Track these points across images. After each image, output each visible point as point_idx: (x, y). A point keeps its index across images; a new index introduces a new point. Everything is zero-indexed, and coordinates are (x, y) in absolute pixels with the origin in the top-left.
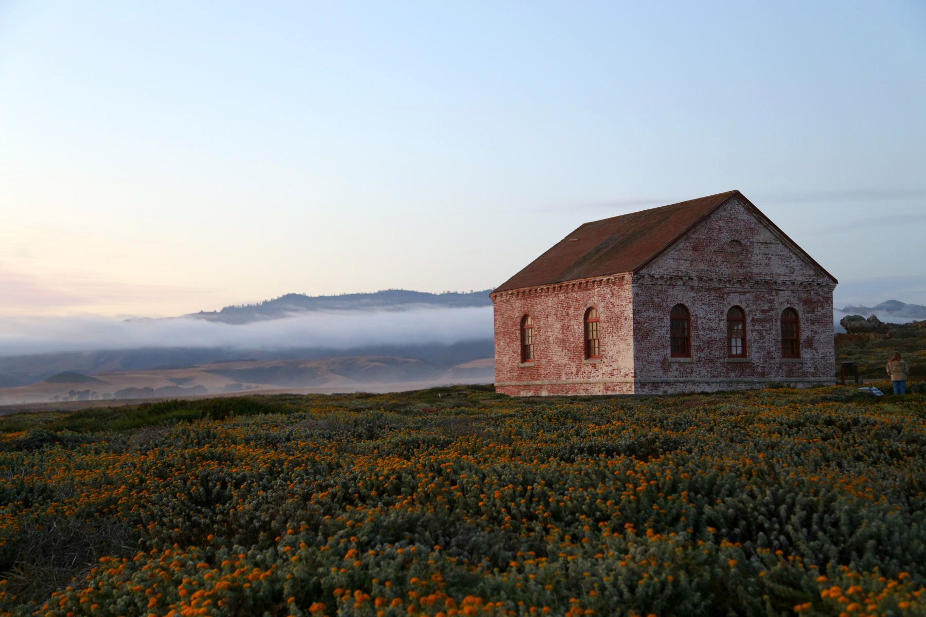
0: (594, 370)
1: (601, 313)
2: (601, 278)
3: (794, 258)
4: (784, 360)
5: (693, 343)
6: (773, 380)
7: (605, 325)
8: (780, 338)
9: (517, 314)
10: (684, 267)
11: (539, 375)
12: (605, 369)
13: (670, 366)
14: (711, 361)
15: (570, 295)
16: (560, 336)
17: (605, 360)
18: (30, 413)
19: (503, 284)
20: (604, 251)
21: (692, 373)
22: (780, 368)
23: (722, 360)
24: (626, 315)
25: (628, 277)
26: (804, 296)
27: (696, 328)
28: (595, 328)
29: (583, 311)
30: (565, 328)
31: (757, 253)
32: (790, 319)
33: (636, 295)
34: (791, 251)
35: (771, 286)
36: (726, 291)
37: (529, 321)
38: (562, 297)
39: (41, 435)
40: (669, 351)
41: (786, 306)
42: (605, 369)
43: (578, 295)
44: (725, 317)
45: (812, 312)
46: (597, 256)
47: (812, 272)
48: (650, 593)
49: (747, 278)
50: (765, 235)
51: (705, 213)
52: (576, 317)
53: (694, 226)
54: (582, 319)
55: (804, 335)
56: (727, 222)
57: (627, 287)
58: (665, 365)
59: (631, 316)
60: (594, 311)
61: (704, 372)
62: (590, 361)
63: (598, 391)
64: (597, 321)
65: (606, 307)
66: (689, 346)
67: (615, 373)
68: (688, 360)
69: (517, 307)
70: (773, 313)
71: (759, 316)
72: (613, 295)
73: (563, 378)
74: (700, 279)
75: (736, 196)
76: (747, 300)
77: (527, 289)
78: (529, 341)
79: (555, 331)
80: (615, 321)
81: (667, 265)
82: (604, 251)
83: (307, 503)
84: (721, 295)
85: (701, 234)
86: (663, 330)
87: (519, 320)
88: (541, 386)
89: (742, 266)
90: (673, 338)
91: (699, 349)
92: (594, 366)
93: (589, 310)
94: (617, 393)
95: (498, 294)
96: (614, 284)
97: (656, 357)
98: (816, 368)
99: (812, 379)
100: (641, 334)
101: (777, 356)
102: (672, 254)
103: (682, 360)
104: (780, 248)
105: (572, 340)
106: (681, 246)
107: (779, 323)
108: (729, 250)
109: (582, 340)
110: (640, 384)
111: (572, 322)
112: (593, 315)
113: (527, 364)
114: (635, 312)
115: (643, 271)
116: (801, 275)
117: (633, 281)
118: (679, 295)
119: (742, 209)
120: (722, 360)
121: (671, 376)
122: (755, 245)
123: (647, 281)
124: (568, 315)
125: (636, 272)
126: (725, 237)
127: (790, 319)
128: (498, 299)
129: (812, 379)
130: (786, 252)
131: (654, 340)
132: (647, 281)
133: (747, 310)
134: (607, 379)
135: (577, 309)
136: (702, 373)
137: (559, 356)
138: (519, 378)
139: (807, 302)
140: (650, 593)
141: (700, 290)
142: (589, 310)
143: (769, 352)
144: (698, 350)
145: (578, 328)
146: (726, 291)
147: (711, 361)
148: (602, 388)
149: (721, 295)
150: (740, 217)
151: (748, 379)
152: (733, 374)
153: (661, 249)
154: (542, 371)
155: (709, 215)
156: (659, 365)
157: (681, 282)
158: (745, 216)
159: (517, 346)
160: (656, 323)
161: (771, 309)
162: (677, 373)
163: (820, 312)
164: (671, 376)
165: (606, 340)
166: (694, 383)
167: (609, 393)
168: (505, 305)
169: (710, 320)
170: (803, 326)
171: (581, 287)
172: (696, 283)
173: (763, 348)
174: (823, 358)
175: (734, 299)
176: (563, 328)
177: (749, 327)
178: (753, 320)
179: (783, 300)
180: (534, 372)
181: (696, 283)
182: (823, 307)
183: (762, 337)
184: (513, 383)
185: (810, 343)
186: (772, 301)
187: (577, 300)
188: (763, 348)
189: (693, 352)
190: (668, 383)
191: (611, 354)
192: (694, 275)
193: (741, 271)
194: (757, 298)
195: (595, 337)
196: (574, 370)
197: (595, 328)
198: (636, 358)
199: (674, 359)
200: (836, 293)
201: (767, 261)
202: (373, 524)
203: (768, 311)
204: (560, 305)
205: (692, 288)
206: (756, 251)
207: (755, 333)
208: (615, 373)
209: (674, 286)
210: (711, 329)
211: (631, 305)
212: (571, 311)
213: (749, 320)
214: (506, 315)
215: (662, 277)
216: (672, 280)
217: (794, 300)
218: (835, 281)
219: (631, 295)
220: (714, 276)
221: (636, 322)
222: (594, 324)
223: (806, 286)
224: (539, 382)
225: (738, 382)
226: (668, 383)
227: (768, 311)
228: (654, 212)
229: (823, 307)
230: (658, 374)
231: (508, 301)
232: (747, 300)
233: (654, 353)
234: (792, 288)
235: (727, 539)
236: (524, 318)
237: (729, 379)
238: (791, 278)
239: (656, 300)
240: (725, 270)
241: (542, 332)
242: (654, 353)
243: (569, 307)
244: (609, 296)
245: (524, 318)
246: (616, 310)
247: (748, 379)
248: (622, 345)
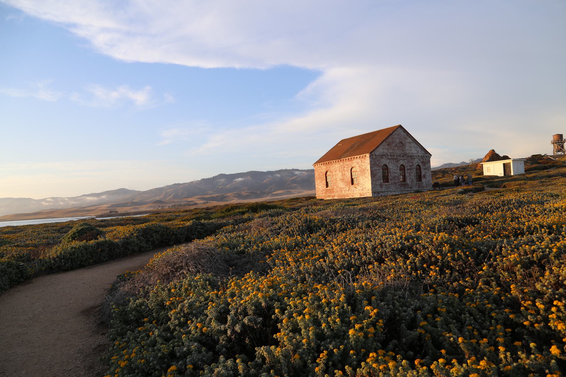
0: (355, 189)
1: (357, 169)
2: (357, 156)
3: (419, 148)
4: (417, 182)
5: (389, 178)
6: (414, 189)
7: (359, 173)
8: (416, 175)
9: (324, 171)
10: (386, 151)
11: (334, 192)
12: (360, 188)
13: (383, 186)
14: (395, 184)
15: (344, 163)
16: (341, 178)
17: (359, 185)
18: (159, 213)
19: (254, 171)
20: (354, 148)
21: (389, 188)
22: (416, 185)
23: (399, 183)
24: (367, 169)
25: (368, 155)
26: (422, 160)
27: (390, 172)
28: (355, 174)
31: (408, 145)
32: (419, 168)
33: (371, 162)
34: (417, 145)
35: (412, 157)
36: (399, 159)
37: (328, 173)
38: (341, 164)
39: (196, 223)
40: (382, 181)
41: (417, 164)
42: (360, 188)
43: (348, 163)
44: (399, 168)
45: (425, 166)
46: (352, 149)
47: (424, 152)
49: (405, 155)
50: (409, 140)
51: (391, 133)
52: (347, 171)
53: (388, 137)
54: (350, 171)
55: (423, 174)
56: (398, 136)
57: (367, 159)
58: (381, 186)
59: (370, 169)
60: (354, 168)
61: (393, 188)
62: (353, 186)
63: (357, 196)
65: (360, 167)
66: (388, 179)
67: (364, 189)
68: (388, 184)
70: (413, 166)
71: (409, 168)
72: (362, 162)
73: (343, 192)
74: (391, 156)
76: (405, 162)
77: (327, 162)
79: (339, 175)
81: (380, 151)
82: (354, 148)
84: (397, 160)
85: (390, 140)
86: (380, 174)
87: (325, 173)
88: (334, 196)
89: (403, 151)
90: (383, 176)
91: (392, 180)
92: (355, 187)
94: (365, 196)
95: (316, 164)
96: (362, 158)
97: (378, 183)
98: (426, 185)
99: (426, 188)
100: (373, 175)
101: (415, 181)
102: (381, 147)
103: (386, 184)
104: (414, 144)
105: (346, 179)
106: (384, 144)
107: (415, 170)
108: (399, 145)
109: (350, 178)
110: (373, 193)
111: (346, 173)
113: (328, 188)
114: (371, 168)
115: (372, 153)
116: (421, 153)
117: (370, 156)
118: (385, 161)
119: (402, 131)
120: (399, 183)
121: (384, 189)
122: (407, 143)
123: (374, 156)
124: (344, 170)
126: (398, 141)
127: (419, 168)
128: (316, 166)
129: (426, 188)
130: (416, 146)
131: (377, 177)
132: (374, 156)
133: (405, 166)
134: (360, 191)
135: (347, 168)
136: (393, 188)
137: (341, 185)
138: (326, 193)
139: (423, 162)
141: (390, 159)
143: (413, 180)
144: (391, 180)
146: (399, 159)
147: (395, 184)
148: (359, 195)
149: (397, 160)
150: (402, 134)
151: (406, 189)
152: (402, 188)
153: (378, 145)
154: (335, 190)
155: (392, 133)
156: (379, 186)
157: (384, 157)
160: (377, 171)
161: (413, 165)
162: (385, 188)
163: (427, 165)
164: (384, 189)
165: (360, 178)
166: (390, 191)
167: (362, 196)
168: (319, 168)
169: (394, 169)
170: (422, 171)
172: (389, 157)
173: (411, 178)
174: (428, 181)
175: (401, 162)
176: (342, 175)
177: (406, 171)
178: (407, 169)
179: (416, 162)
180: (332, 191)
181: (389, 157)
182: (427, 164)
183: (410, 175)
184: (324, 195)
185: (424, 176)
186: (412, 163)
187: (347, 165)
188: (411, 178)
189: (390, 181)
190: (382, 192)
191: (362, 183)
192: (389, 154)
193: (403, 152)
194: (408, 162)
195: (355, 177)
196: (347, 189)
197: (355, 174)
198: (372, 184)
199: (384, 184)
200: (432, 159)
201: (410, 149)
203: (411, 166)
204: (341, 167)
205: (388, 158)
206: (407, 145)
207: (408, 174)
208: (364, 189)
209: (382, 158)
210: (395, 173)
211: (369, 165)
212: (345, 169)
213: (406, 169)
214: (319, 172)
215: (379, 155)
216: (382, 156)
217: (419, 162)
218: (431, 155)
219: (369, 162)
220: (395, 154)
221: (371, 171)
222: (355, 173)
224: (334, 194)
225: (404, 190)
226: (382, 192)
227: (411, 166)
228: (379, 132)
229: (427, 164)
230: (379, 189)
231: (320, 167)
232: (405, 162)
233: (377, 182)
234: (418, 158)
237: (401, 190)
238: (418, 154)
239: (377, 163)
240: (398, 152)
241: (334, 177)
242: (377, 182)
243: (345, 167)
244: (360, 163)
246: (363, 167)
247: (406, 189)
248: (366, 179)
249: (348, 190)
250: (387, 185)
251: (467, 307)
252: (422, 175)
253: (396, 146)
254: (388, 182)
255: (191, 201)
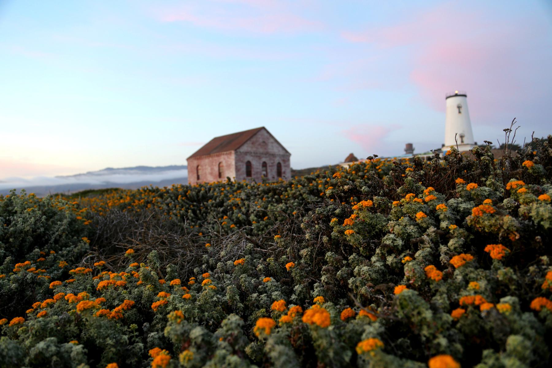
1: (224, 164)
10: (249, 149)
29: (218, 163)
30: (212, 169)
32: (279, 166)
33: (236, 158)
35: (274, 155)
37: (199, 167)
43: (216, 158)
48: (349, 294)
50: (272, 140)
54: (217, 166)
64: (223, 166)
69: (195, 163)
71: (271, 164)
75: (263, 128)
78: (200, 173)
79: (208, 170)
80: (229, 166)
81: (245, 148)
83: (289, 306)
84: (260, 158)
85: (254, 139)
86: (244, 169)
91: (254, 175)
93: (220, 163)
97: (242, 177)
112: (221, 165)
114: (236, 163)
116: (282, 152)
118: (248, 158)
123: (239, 153)
125: (236, 150)
126: (261, 140)
127: (279, 166)
132: (239, 153)
140: (349, 294)
142: (220, 163)
145: (216, 169)
149: (260, 158)
158: (266, 134)
159: (195, 175)
171: (218, 156)
175: (264, 160)
179: (277, 160)
181: (253, 154)
185: (284, 173)
202: (548, 287)
216: (246, 153)
223: (283, 156)
235: (495, 233)
236: (198, 166)
240: (261, 150)
245: (198, 166)
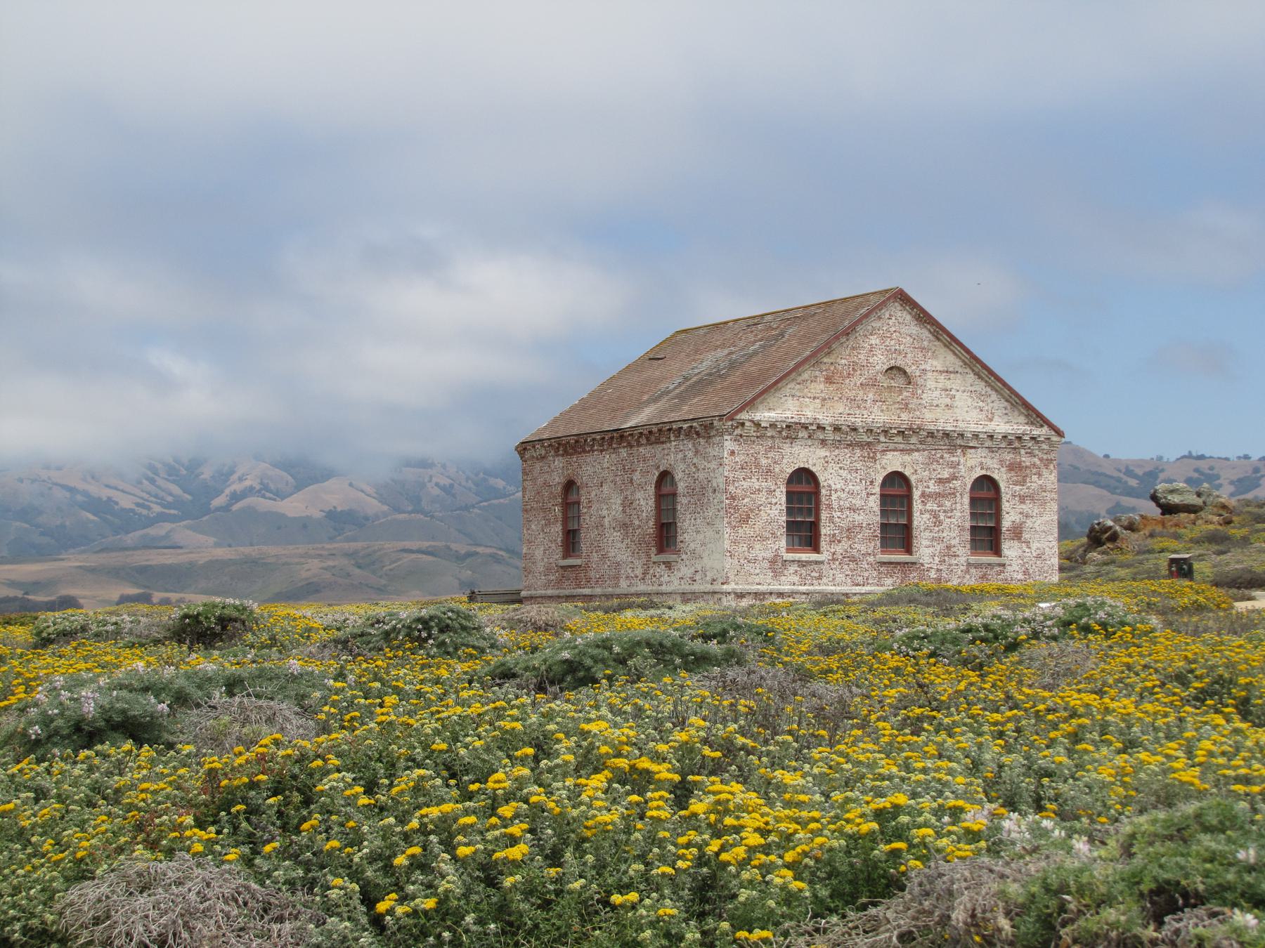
4: (973, 559)
5: (823, 531)
9: (557, 479)
14: (853, 559)
16: (620, 516)
21: (820, 578)
27: (829, 506)
34: (988, 384)
45: (1022, 483)
67: (697, 577)
68: (813, 557)
70: (957, 483)
71: (933, 488)
73: (623, 584)
89: (906, 407)
91: (834, 540)
98: (1026, 572)
105: (637, 522)
119: (908, 317)
120: (871, 559)
122: (929, 374)
131: (759, 525)
133: (913, 479)
138: (559, 583)
147: (853, 559)
160: (762, 498)
161: (954, 478)
174: (1038, 557)
175: (893, 462)
178: (923, 495)
181: (830, 435)
185: (1017, 533)
186: (955, 465)
189: (823, 544)
191: (692, 546)
196: (639, 572)
199: (790, 556)
201: (948, 401)
203: (948, 480)
206: (931, 384)
207: (927, 516)
208: (697, 577)
210: (853, 509)
213: (916, 494)
214: (540, 481)
227: (948, 480)
232: (916, 462)
233: (758, 546)
239: (764, 462)
242: (758, 546)
249: (641, 576)
250: (809, 563)
251: (36, 705)
252: (1006, 523)
253: (872, 384)
254: (816, 549)
255: (37, 585)
